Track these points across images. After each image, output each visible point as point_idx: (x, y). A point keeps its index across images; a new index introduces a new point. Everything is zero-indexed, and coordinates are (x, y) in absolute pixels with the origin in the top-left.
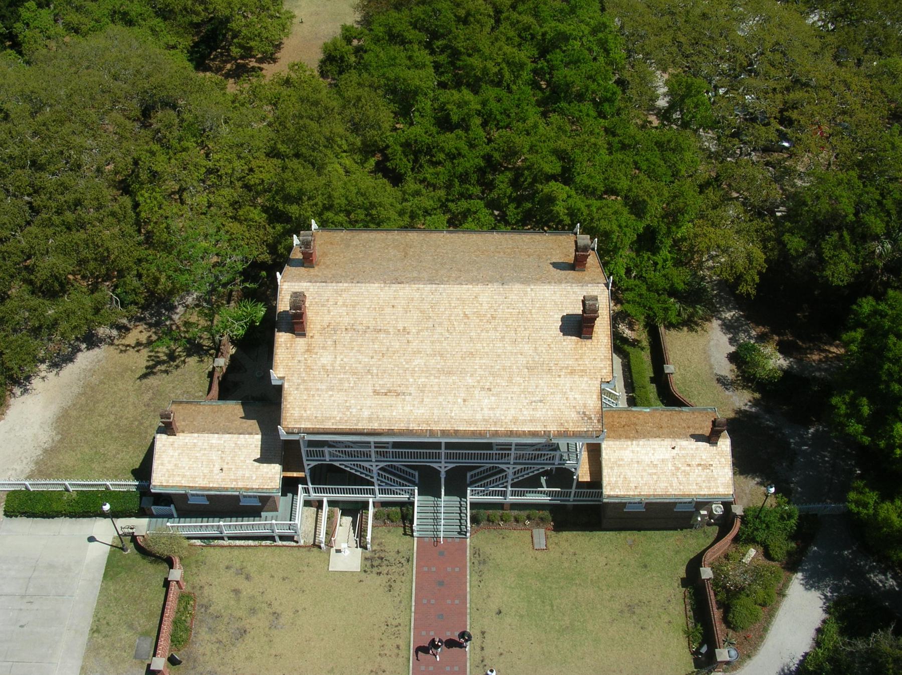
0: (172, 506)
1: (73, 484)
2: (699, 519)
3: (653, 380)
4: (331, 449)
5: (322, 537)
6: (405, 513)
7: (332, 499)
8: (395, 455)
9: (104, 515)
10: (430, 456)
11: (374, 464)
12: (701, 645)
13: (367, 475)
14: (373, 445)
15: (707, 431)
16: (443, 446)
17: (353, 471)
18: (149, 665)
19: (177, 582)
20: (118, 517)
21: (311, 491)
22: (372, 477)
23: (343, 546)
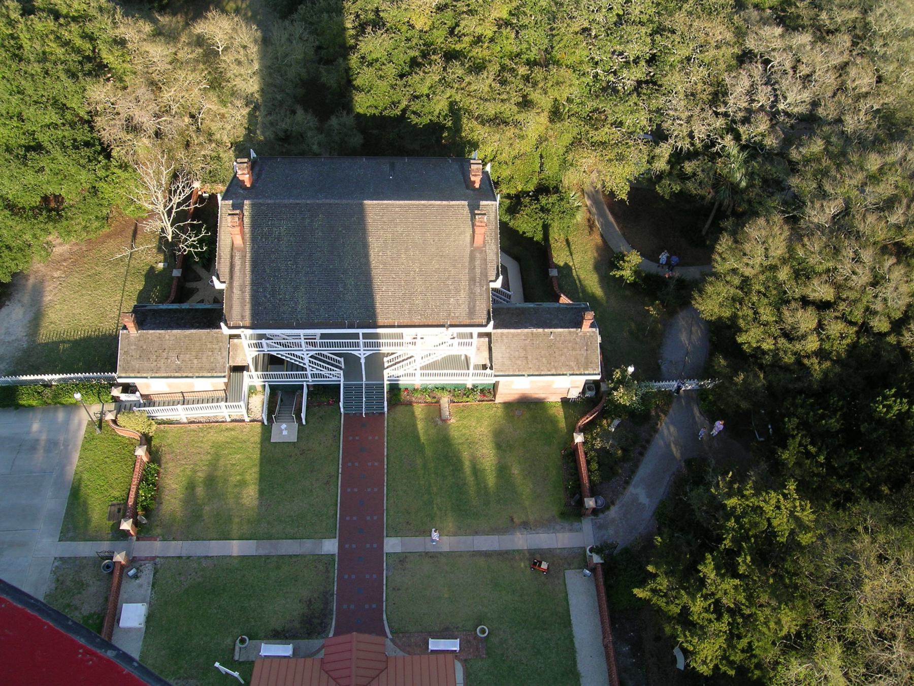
4: (268, 341)
11: (305, 353)
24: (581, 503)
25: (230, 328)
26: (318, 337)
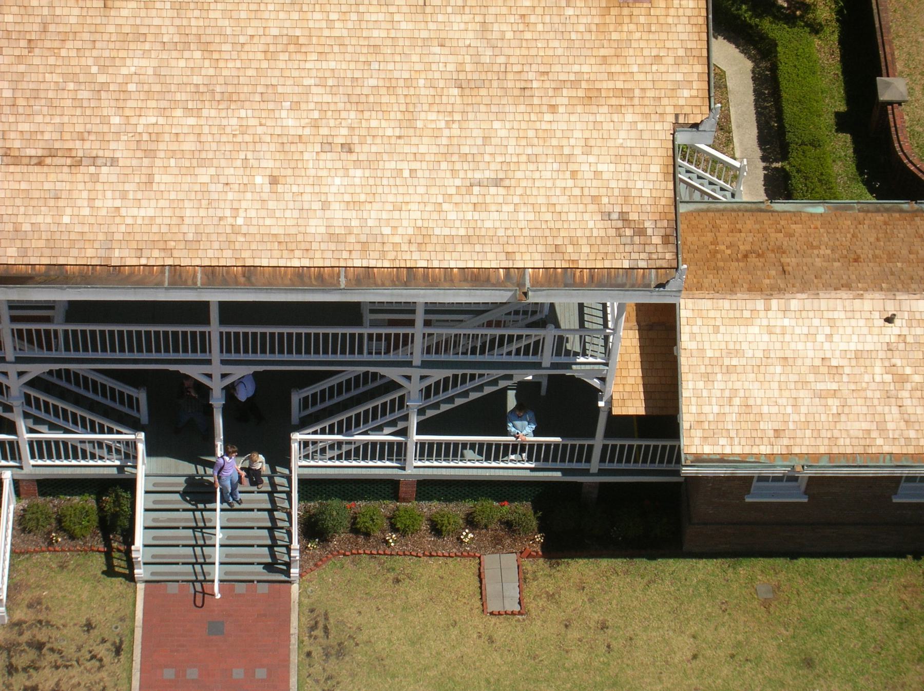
26: (59, 314)
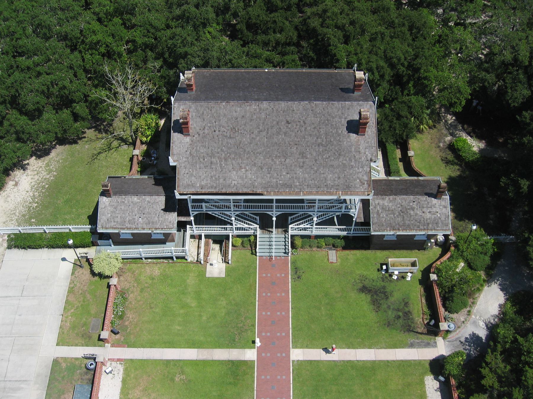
0: (111, 240)
1: (50, 229)
2: (429, 244)
3: (401, 160)
4: (206, 204)
5: (202, 256)
6: (250, 242)
7: (207, 234)
8: (245, 207)
9: (69, 247)
10: (266, 207)
11: (233, 213)
12: (430, 320)
13: (228, 219)
14: (232, 201)
15: (435, 191)
16: (274, 201)
17: (220, 217)
18: (100, 335)
19: (115, 285)
20: (77, 247)
21: (194, 229)
22: (231, 221)
23: (214, 262)
24: (437, 326)
25: (181, 194)
